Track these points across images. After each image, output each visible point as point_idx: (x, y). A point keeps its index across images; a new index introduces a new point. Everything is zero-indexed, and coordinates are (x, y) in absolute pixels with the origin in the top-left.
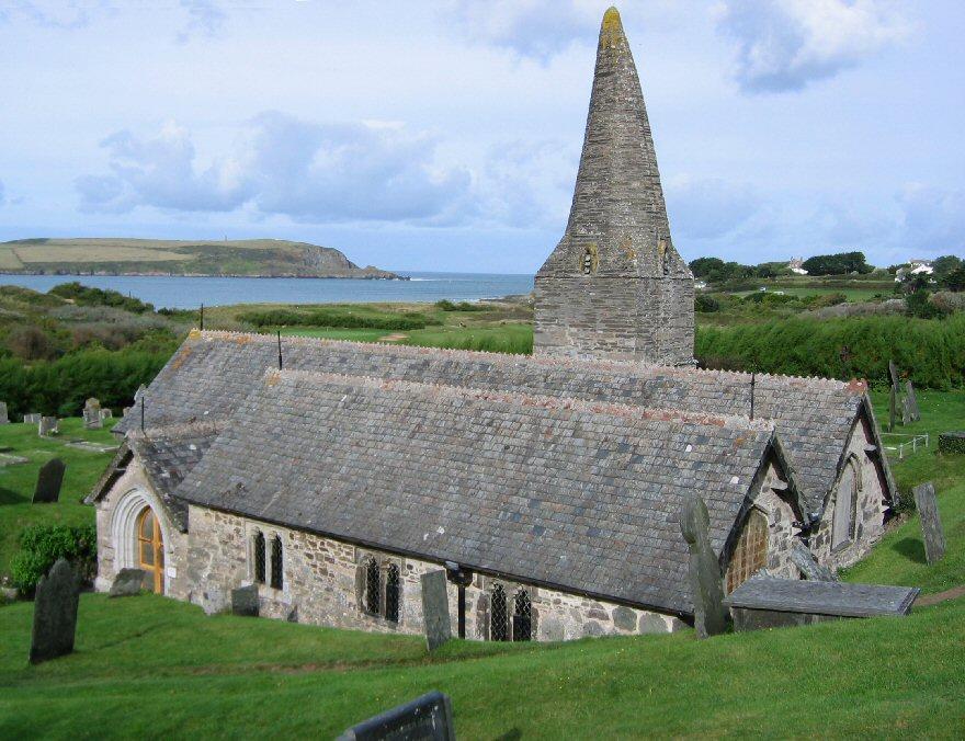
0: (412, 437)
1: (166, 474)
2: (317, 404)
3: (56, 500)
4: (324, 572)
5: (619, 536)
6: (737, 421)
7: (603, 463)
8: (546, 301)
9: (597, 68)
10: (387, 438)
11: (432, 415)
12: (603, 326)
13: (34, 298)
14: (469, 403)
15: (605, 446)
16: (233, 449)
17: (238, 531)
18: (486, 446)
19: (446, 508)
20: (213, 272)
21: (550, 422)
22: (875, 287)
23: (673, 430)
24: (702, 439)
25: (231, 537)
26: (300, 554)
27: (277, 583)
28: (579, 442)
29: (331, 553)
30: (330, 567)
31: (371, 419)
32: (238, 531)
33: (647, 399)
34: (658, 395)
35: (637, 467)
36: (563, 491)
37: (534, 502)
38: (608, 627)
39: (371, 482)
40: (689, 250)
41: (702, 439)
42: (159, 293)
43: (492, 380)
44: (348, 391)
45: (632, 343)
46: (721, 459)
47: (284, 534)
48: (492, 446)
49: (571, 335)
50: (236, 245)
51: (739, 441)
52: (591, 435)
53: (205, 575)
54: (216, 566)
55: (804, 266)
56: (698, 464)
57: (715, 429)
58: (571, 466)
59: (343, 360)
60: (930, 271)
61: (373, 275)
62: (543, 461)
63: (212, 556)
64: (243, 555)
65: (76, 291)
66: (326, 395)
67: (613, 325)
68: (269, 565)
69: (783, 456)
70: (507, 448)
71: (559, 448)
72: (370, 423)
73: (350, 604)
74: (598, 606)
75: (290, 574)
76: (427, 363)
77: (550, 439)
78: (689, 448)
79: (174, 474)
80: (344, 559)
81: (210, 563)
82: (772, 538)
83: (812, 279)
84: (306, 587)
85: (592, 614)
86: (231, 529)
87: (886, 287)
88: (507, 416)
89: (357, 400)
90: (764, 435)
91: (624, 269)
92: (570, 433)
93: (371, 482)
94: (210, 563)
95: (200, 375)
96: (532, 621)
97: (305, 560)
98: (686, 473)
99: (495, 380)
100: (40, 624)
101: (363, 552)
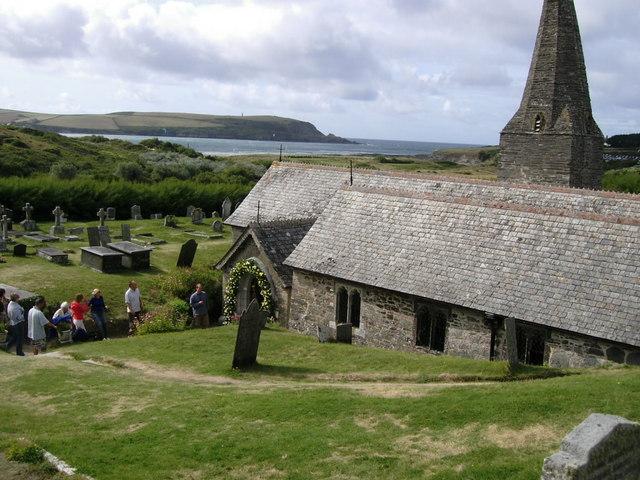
1: (273, 251)
4: (391, 317)
5: (609, 300)
8: (508, 149)
12: (548, 166)
16: (323, 236)
28: (573, 237)
29: (396, 305)
47: (171, 325)
52: (581, 233)
54: (312, 310)
58: (568, 253)
64: (332, 304)
65: (157, 143)
70: (520, 239)
72: (420, 221)
74: (597, 346)
79: (278, 251)
88: (519, 219)
92: (565, 231)
93: (424, 259)
96: (545, 354)
101: (420, 306)
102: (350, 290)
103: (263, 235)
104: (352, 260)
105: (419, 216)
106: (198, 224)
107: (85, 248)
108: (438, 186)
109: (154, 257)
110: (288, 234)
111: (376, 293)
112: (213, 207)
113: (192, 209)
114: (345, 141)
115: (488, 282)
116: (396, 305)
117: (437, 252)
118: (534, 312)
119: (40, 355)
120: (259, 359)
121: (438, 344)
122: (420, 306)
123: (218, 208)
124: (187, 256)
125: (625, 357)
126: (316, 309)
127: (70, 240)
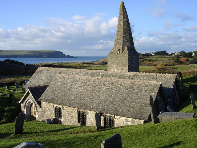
0: (87, 87)
2: (67, 81)
4: (70, 115)
6: (153, 82)
7: (127, 91)
10: (82, 87)
11: (91, 82)
14: (99, 80)
15: (127, 88)
18: (103, 88)
19: (95, 101)
21: (116, 83)
23: (140, 84)
24: (146, 86)
28: (122, 87)
31: (79, 84)
33: (133, 79)
34: (135, 78)
35: (134, 92)
36: (119, 97)
37: (113, 99)
38: (130, 124)
39: (80, 96)
41: (146, 86)
42: (26, 61)
43: (101, 75)
44: (74, 78)
46: (151, 90)
48: (104, 88)
49: (116, 67)
51: (154, 86)
56: (146, 91)
57: (149, 84)
59: (71, 72)
61: (69, 56)
62: (115, 91)
63: (47, 112)
66: (69, 79)
68: (58, 112)
69: (21, 76)
70: (107, 89)
71: (118, 88)
73: (76, 121)
75: (63, 115)
76: (88, 73)
77: (116, 87)
78: (144, 88)
80: (74, 112)
82: (160, 105)
84: (67, 118)
89: (76, 80)
90: (159, 85)
92: (120, 85)
95: (41, 76)
99: (102, 76)
103: (117, 44)
104: (59, 98)
105: (79, 83)
109: (137, 47)
110: (41, 90)
114: (73, 57)
115: (97, 102)
117: (84, 94)
120: (25, 131)
121: (79, 113)
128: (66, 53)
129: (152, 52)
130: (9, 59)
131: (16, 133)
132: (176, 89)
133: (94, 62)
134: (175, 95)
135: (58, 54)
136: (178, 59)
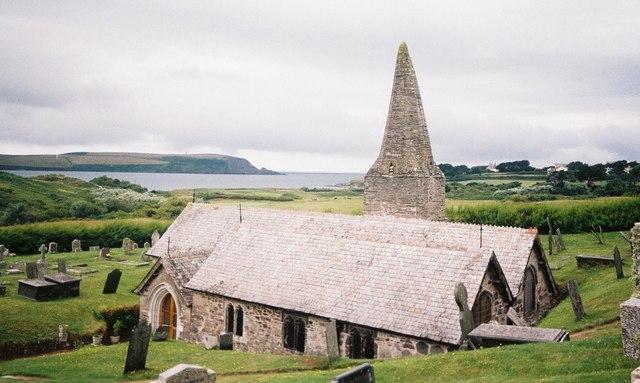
3: (114, 291)
4: (265, 326)
9: (396, 73)
10: (297, 257)
13: (86, 185)
17: (220, 305)
20: (179, 171)
22: (535, 179)
25: (216, 309)
26: (253, 317)
27: (240, 333)
29: (269, 316)
30: (268, 324)
32: (220, 305)
40: (438, 163)
45: (415, 209)
47: (243, 306)
50: (201, 157)
53: (200, 329)
54: (207, 324)
55: (497, 168)
60: (566, 170)
61: (265, 172)
67: (404, 200)
75: (247, 328)
81: (203, 323)
82: (494, 308)
83: (500, 175)
85: (405, 346)
86: (216, 304)
87: (542, 178)
91: (410, 172)
94: (203, 323)
97: (255, 320)
98: (450, 274)
100: (130, 351)
101: (286, 316)
102: (235, 306)
103: (387, 150)
106: (130, 254)
107: (22, 281)
108: (312, 220)
111: (255, 307)
112: (143, 239)
113: (126, 241)
114: (276, 173)
116: (269, 316)
118: (363, 317)
119: (81, 351)
121: (301, 347)
122: (286, 316)
123: (149, 240)
124: (112, 283)
125: (429, 350)
126: (214, 320)
127: (11, 274)
128: (257, 160)
129: (491, 163)
130: (105, 176)
131: (128, 369)
132: (537, 267)
133: (331, 188)
134: (535, 282)
135: (240, 167)
136: (561, 185)
